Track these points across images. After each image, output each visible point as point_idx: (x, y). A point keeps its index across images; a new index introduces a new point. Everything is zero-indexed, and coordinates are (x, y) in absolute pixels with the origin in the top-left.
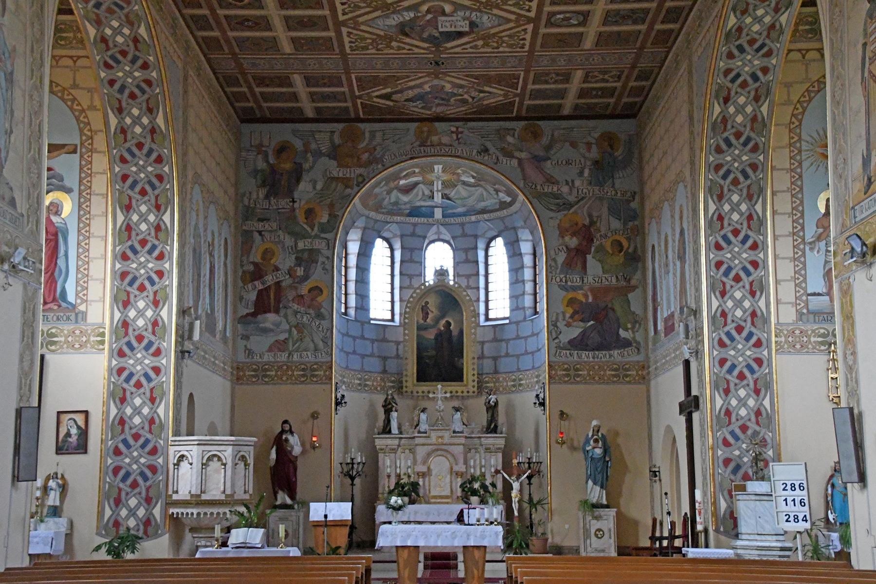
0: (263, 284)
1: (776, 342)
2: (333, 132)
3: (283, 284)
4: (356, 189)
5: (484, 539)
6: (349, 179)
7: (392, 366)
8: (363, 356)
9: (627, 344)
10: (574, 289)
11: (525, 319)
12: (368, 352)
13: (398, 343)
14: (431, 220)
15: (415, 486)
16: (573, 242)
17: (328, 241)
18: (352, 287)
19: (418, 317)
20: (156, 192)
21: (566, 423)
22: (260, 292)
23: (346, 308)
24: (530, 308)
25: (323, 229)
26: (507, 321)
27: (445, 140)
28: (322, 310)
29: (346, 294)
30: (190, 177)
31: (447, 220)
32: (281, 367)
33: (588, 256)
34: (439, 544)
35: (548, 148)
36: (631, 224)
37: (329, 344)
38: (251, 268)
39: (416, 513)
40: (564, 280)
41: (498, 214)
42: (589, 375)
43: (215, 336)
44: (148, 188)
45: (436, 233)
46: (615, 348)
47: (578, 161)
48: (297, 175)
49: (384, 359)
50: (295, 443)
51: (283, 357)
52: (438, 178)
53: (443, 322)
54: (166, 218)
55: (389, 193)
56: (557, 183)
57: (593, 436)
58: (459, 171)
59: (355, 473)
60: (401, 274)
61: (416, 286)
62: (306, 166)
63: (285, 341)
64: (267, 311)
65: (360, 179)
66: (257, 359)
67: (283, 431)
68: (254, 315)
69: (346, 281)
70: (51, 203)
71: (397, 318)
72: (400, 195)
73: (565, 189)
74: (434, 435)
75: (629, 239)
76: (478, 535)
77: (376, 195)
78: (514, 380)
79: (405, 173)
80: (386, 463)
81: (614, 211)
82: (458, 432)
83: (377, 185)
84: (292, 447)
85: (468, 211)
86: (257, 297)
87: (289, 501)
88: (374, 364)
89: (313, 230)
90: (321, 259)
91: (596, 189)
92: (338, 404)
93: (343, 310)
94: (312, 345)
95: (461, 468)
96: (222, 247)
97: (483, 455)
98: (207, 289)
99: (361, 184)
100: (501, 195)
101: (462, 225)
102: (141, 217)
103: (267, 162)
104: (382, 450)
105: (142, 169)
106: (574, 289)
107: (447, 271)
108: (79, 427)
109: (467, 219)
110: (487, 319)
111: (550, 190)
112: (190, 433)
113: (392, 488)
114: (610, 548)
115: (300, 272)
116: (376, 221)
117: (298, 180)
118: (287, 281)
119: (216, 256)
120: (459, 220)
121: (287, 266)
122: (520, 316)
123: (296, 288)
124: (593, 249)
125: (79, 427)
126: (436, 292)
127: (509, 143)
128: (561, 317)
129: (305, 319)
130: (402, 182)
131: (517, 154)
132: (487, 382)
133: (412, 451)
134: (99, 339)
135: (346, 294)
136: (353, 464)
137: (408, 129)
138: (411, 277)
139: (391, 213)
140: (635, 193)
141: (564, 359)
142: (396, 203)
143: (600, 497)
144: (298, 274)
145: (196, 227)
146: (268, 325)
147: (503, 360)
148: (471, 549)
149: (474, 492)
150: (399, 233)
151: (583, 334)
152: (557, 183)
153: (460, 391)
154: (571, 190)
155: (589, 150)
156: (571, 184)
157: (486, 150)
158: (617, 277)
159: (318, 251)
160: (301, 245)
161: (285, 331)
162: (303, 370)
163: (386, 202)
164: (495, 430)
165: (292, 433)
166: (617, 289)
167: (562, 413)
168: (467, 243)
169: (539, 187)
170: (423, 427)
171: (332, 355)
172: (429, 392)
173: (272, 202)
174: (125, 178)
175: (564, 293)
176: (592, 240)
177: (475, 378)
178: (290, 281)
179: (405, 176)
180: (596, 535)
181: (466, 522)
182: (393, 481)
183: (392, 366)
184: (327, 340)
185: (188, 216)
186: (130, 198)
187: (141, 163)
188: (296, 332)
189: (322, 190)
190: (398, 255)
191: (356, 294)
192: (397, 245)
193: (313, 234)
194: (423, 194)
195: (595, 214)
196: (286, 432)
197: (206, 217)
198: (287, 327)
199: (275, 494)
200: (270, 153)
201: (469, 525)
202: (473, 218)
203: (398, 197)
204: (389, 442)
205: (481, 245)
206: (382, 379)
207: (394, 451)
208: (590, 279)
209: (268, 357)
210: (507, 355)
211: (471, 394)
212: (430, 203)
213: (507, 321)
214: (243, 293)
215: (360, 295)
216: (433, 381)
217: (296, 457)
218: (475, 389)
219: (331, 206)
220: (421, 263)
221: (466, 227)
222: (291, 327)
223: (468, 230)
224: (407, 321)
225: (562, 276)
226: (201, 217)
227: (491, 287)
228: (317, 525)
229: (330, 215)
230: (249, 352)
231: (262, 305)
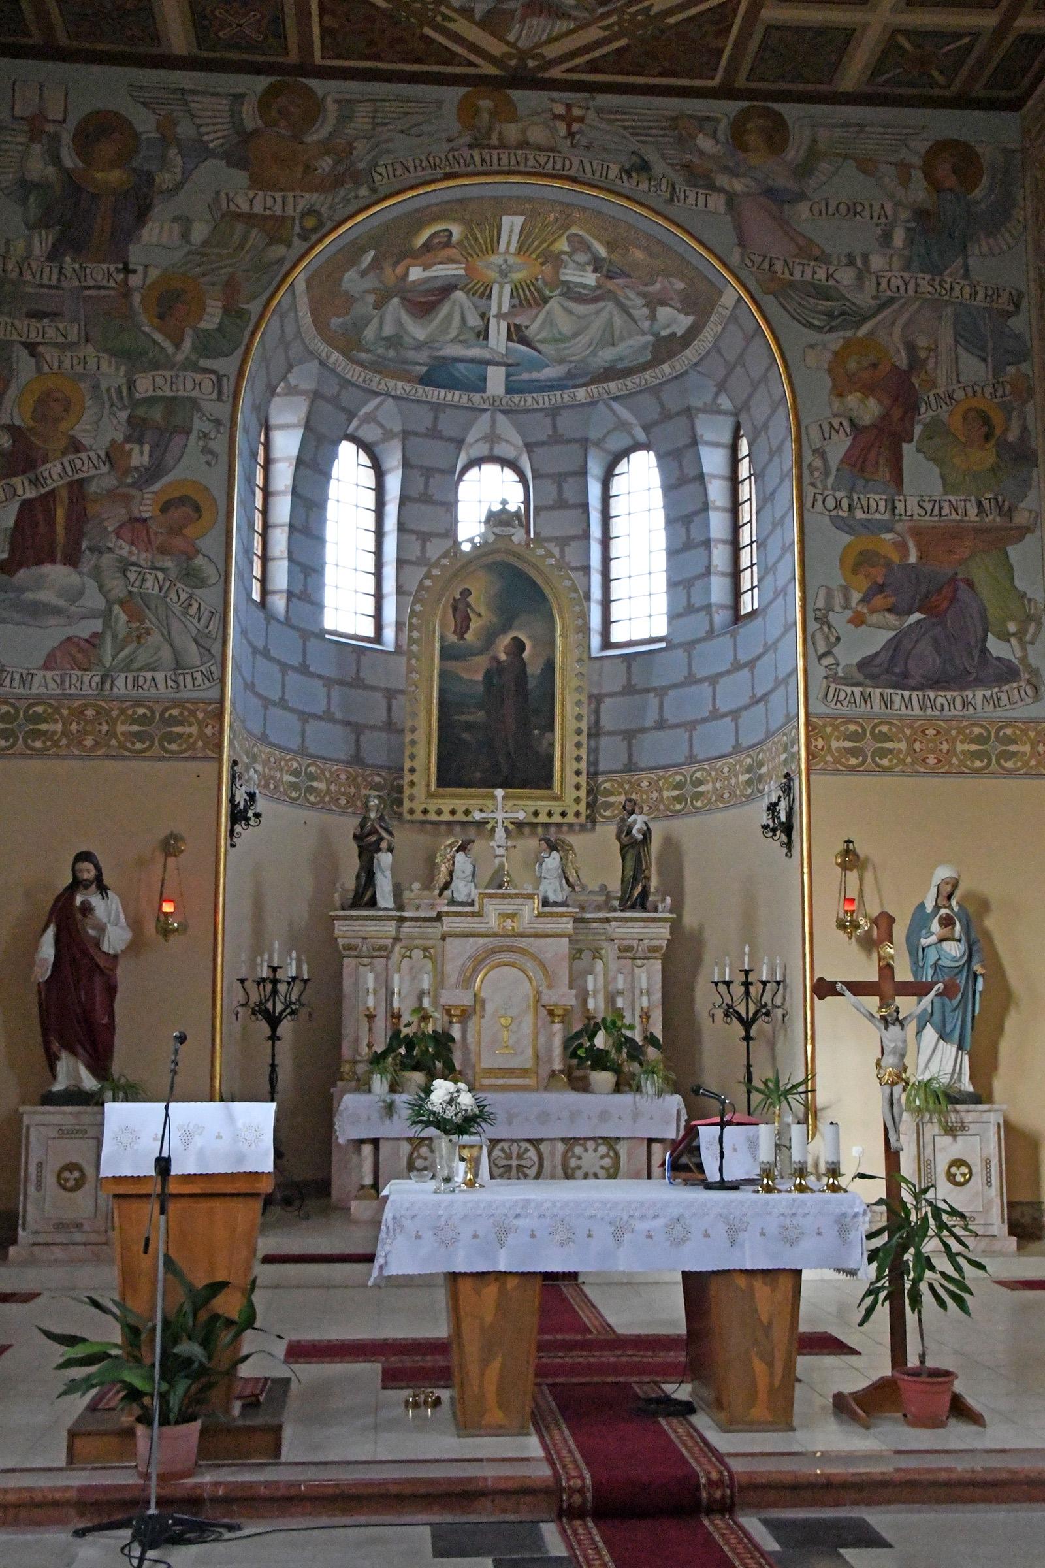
0: (35, 482)
2: (238, 98)
3: (93, 488)
4: (298, 245)
5: (792, 1243)
6: (281, 220)
7: (375, 747)
8: (305, 717)
9: (1007, 673)
11: (711, 634)
12: (319, 709)
13: (390, 694)
14: (476, 398)
15: (443, 1041)
16: (869, 410)
17: (220, 378)
18: (280, 540)
19: (440, 626)
23: (264, 592)
24: (722, 607)
25: (208, 346)
26: (663, 645)
27: (537, 134)
29: (265, 559)
33: (905, 446)
35: (804, 170)
36: (1011, 369)
37: (216, 649)
40: (845, 504)
45: (485, 438)
46: (979, 682)
47: (876, 207)
48: (139, 204)
49: (357, 729)
50: (111, 921)
53: (505, 641)
56: (823, 258)
57: (937, 908)
59: (280, 1007)
60: (401, 528)
62: (165, 179)
63: (94, 641)
64: (45, 556)
65: (310, 222)
67: (77, 884)
69: (266, 526)
71: (389, 634)
72: (405, 318)
73: (846, 276)
74: (492, 910)
75: (1007, 409)
76: (772, 1228)
78: (679, 786)
80: (364, 985)
81: (968, 335)
82: (556, 904)
84: (102, 929)
85: (570, 375)
86: (19, 519)
87: (89, 1082)
88: (332, 741)
89: (178, 346)
90: (198, 424)
91: (924, 280)
92: (238, 816)
93: (256, 596)
94: (166, 654)
95: (563, 996)
97: (613, 966)
99: (312, 234)
101: (553, 412)
103: (56, 160)
104: (349, 947)
109: (567, 396)
110: (607, 644)
111: (808, 276)
113: (380, 1048)
114: (986, 1210)
115: (140, 457)
116: (346, 383)
117: (142, 216)
118: (103, 480)
120: (545, 400)
121: (104, 442)
122: (696, 625)
123: (127, 499)
124: (918, 429)
126: (489, 567)
127: (702, 153)
128: (838, 601)
129: (149, 584)
130: (416, 273)
131: (722, 180)
132: (609, 793)
135: (265, 559)
136: (275, 982)
137: (440, 103)
138: (425, 538)
139: (378, 367)
140: (1020, 294)
141: (845, 710)
142: (394, 342)
143: (956, 1073)
144: (135, 461)
146: (46, 596)
147: (647, 740)
148: (741, 1282)
149: (600, 1060)
150: (397, 428)
151: (894, 646)
152: (823, 258)
154: (860, 278)
155: (905, 181)
156: (858, 263)
157: (644, 167)
158: (980, 504)
159: (194, 403)
160: (144, 386)
161: (93, 615)
163: (369, 334)
164: (642, 903)
165: (103, 889)
166: (980, 531)
168: (560, 459)
169: (779, 266)
170: (462, 889)
171: (222, 681)
173: (69, 272)
177: (582, 780)
178: (110, 482)
179: (427, 247)
180: (951, 1178)
181: (712, 1175)
182: (381, 1024)
183: (375, 747)
184: (212, 644)
188: (123, 618)
189: (206, 243)
190: (394, 484)
191: (294, 493)
192: (393, 462)
193: (180, 357)
194: (463, 320)
195: (922, 341)
196: (86, 885)
198: (101, 604)
199: (52, 1061)
200: (66, 138)
201: (723, 1185)
202: (581, 394)
203: (399, 323)
204: (372, 928)
205: (595, 468)
206: (351, 780)
207: (383, 952)
208: (912, 502)
209: (45, 684)
210: (661, 725)
211: (570, 818)
212: (475, 352)
213: (663, 645)
215: (299, 564)
217: (115, 957)
218: (582, 808)
219: (230, 288)
221: (560, 421)
222: (110, 604)
223: (567, 424)
225: (839, 495)
227: (616, 569)
228: (127, 1191)
229: (227, 311)
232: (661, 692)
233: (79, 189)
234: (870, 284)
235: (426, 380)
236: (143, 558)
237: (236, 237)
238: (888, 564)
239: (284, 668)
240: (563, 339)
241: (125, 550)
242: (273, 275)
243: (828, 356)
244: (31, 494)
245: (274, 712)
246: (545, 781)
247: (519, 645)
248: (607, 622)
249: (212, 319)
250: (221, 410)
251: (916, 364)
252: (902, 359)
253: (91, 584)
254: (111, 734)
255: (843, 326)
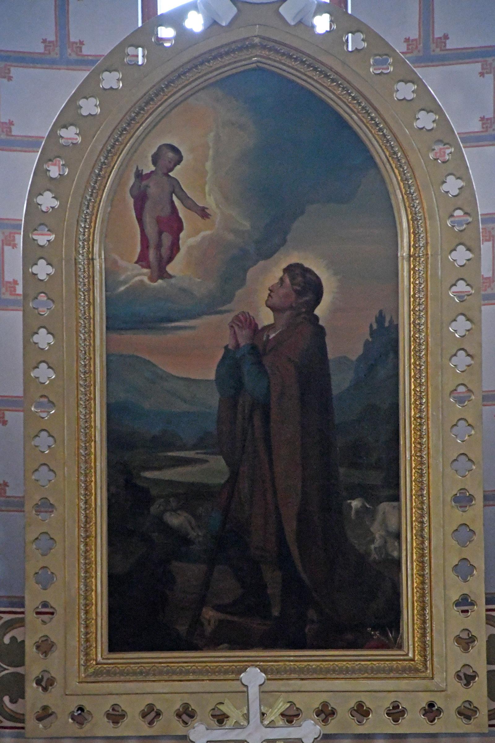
19: (111, 253)
61: (99, 46)
126: (229, 85)
153: (379, 706)
172: (186, 714)
216: (213, 643)
224: (42, 270)
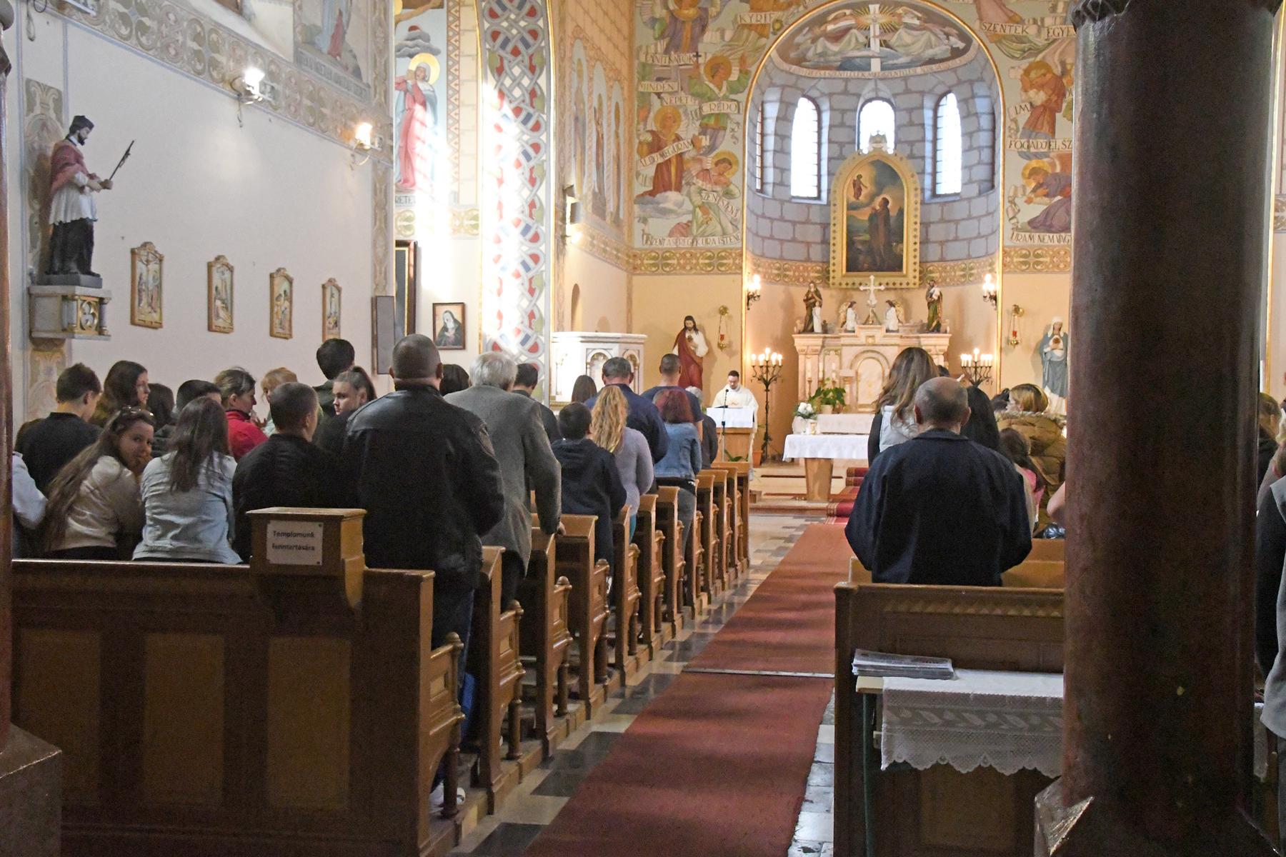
0: (662, 155)
1: (1276, 218)
3: (686, 157)
4: (772, 37)
6: (764, 26)
10: (1038, 156)
14: (866, 74)
15: (839, 392)
16: (1039, 97)
20: (531, 51)
21: (1022, 319)
22: (659, 166)
23: (763, 184)
25: (733, 90)
28: (732, 187)
30: (569, 32)
31: (887, 73)
32: (684, 255)
34: (854, 457)
38: (649, 138)
39: (839, 424)
41: (951, 64)
42: (1052, 262)
43: (604, 218)
44: (521, 47)
51: (686, 242)
52: (875, 21)
53: (879, 200)
54: (542, 81)
55: (814, 41)
56: (1021, 21)
58: (900, 11)
60: (830, 141)
62: (713, 11)
63: (689, 224)
64: (667, 188)
65: (777, 26)
66: (656, 245)
68: (652, 193)
69: (763, 151)
70: (418, 68)
71: (824, 195)
72: (828, 44)
73: (1032, 30)
77: (799, 45)
78: (963, 270)
79: (833, 16)
83: (799, 30)
90: (730, 126)
93: (758, 187)
94: (719, 228)
96: (613, 115)
98: (594, 164)
100: (952, 39)
101: (905, 79)
102: (514, 81)
103: (667, 8)
105: (514, 24)
106: (1038, 156)
107: (884, 137)
108: (455, 321)
112: (572, 329)
115: (705, 141)
117: (703, 29)
118: (690, 153)
119: (605, 125)
121: (690, 136)
125: (455, 321)
128: (1020, 192)
130: (830, 27)
133: (838, 352)
134: (473, 222)
145: (579, 89)
146: (669, 205)
151: (1047, 213)
152: (1021, 21)
159: (727, 115)
160: (706, 109)
161: (688, 212)
162: (709, 258)
164: (937, 329)
165: (695, 329)
167: (1017, 309)
169: (998, 28)
170: (850, 324)
174: (495, 35)
175: (1025, 162)
176: (1064, 95)
177: (917, 267)
178: (693, 153)
179: (835, 19)
185: (567, 79)
186: (501, 59)
187: (513, 16)
195: (1069, 60)
197: (591, 79)
202: (919, 70)
208: (1059, 143)
209: (669, 243)
210: (956, 239)
214: (640, 168)
218: (917, 280)
220: (854, 129)
221: (909, 82)
222: (695, 207)
223: (913, 85)
226: (585, 79)
230: (648, 238)
231: (662, 183)
232: (957, 222)
233: (676, 19)
234: (1044, 32)
235: (841, 68)
236: (709, 187)
237: (744, 37)
238: (1046, 173)
239: (772, 220)
240: (907, 45)
241: (700, 183)
242: (760, 50)
243: (1021, 72)
244: (661, 160)
245: (767, 242)
246: (900, 268)
247: (886, 202)
248: (934, 183)
249: (734, 76)
250: (739, 118)
251: (1065, 72)
252: (1058, 70)
253: (687, 199)
254: (697, 264)
255: (1029, 57)
